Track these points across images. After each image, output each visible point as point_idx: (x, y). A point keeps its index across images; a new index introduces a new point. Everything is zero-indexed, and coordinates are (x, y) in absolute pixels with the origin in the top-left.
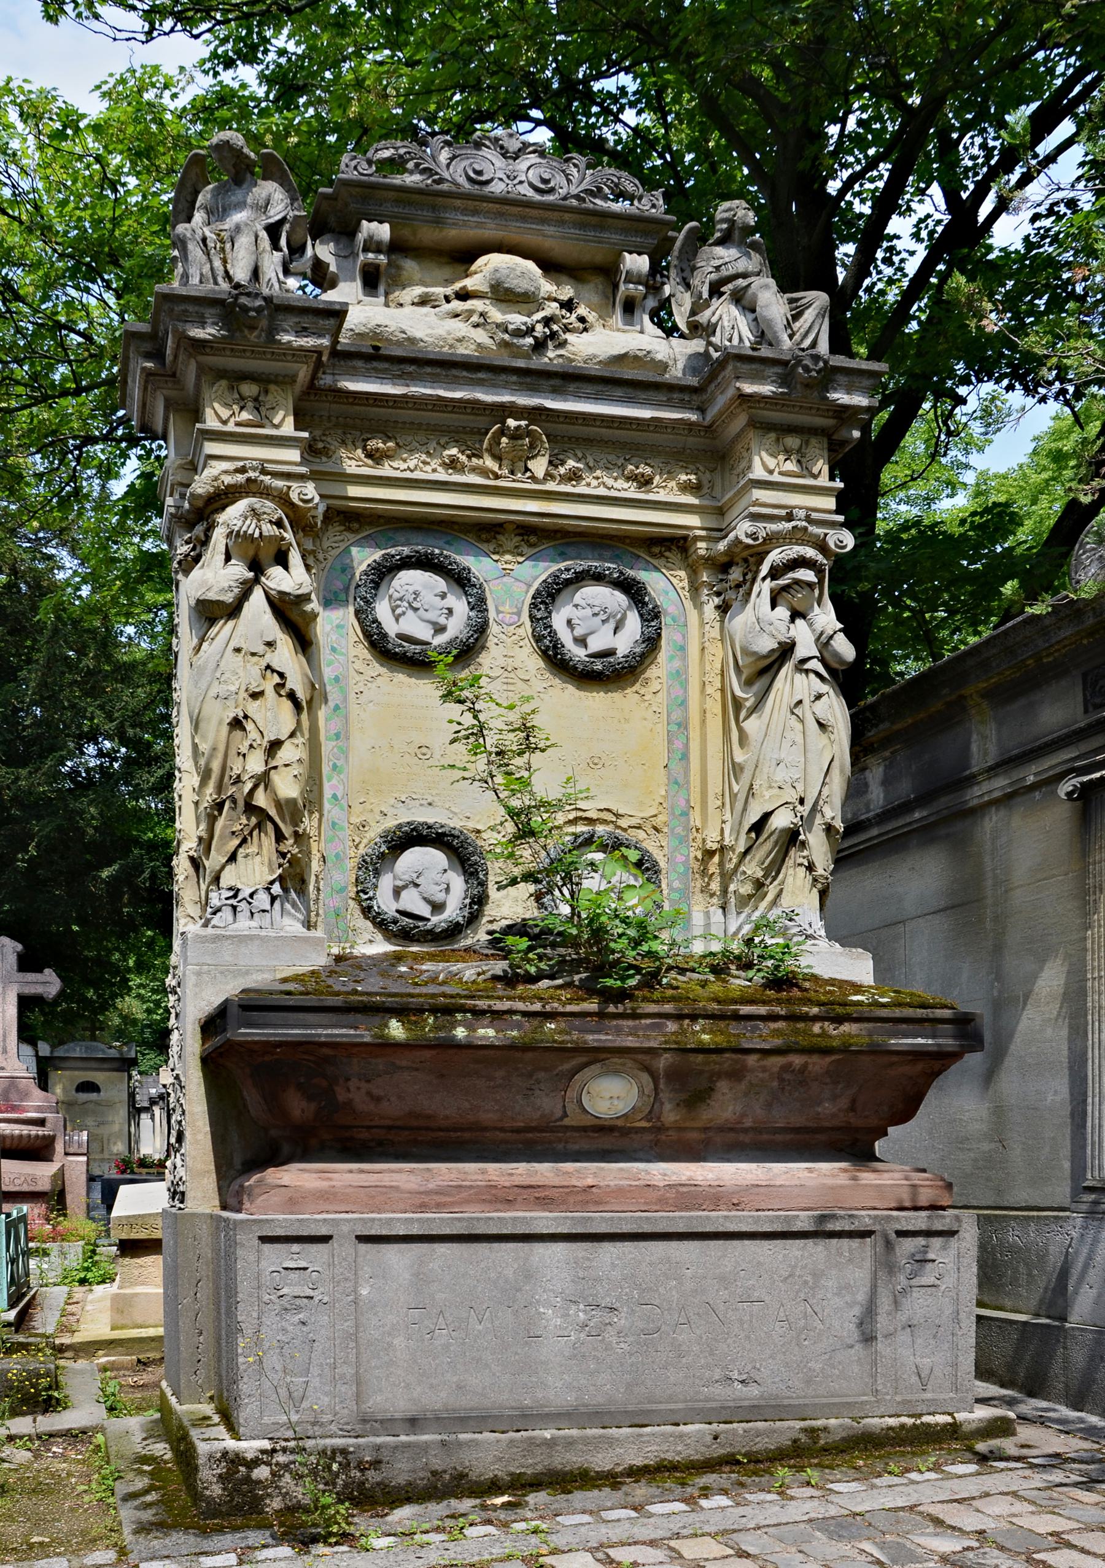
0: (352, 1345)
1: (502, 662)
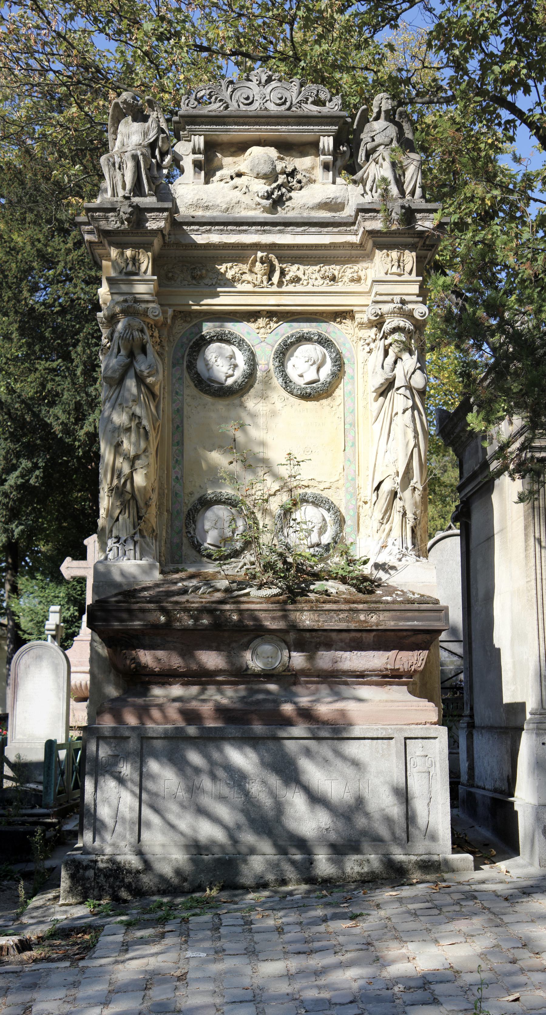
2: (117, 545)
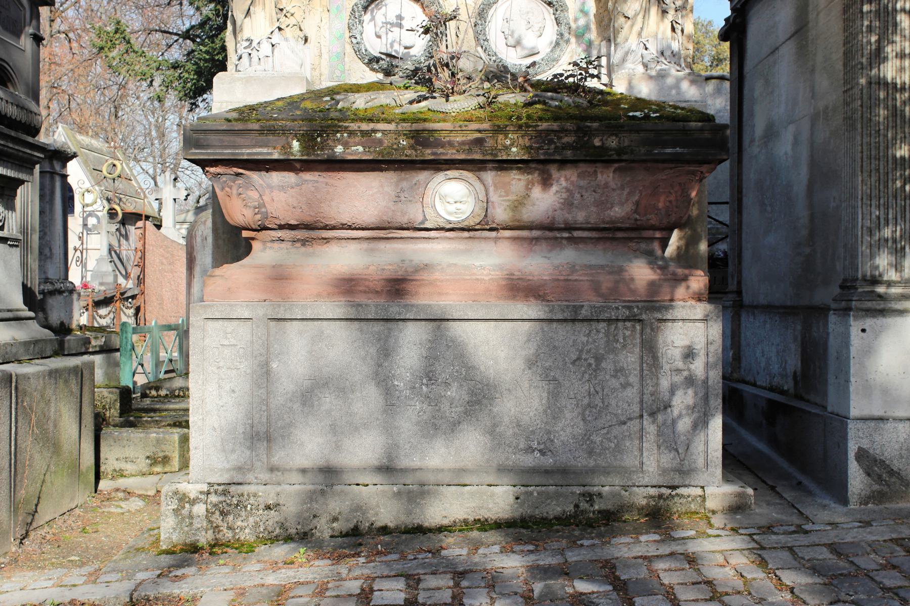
0: (264, 408)
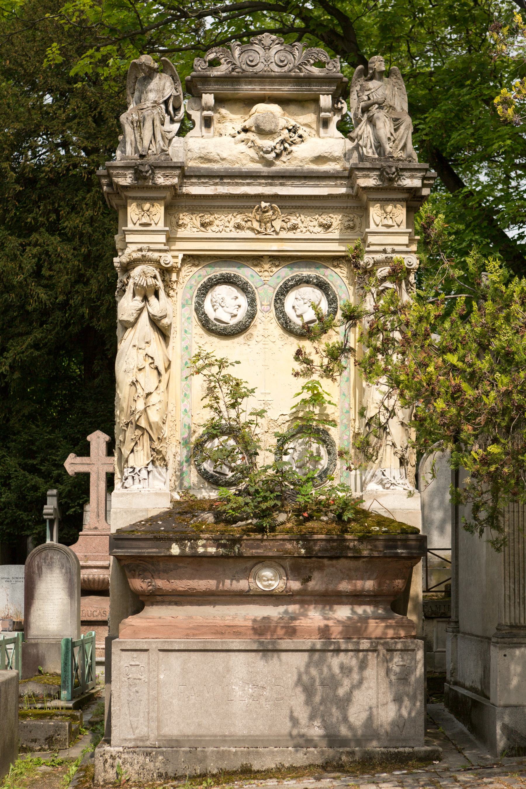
1: (262, 332)
2: (132, 474)
